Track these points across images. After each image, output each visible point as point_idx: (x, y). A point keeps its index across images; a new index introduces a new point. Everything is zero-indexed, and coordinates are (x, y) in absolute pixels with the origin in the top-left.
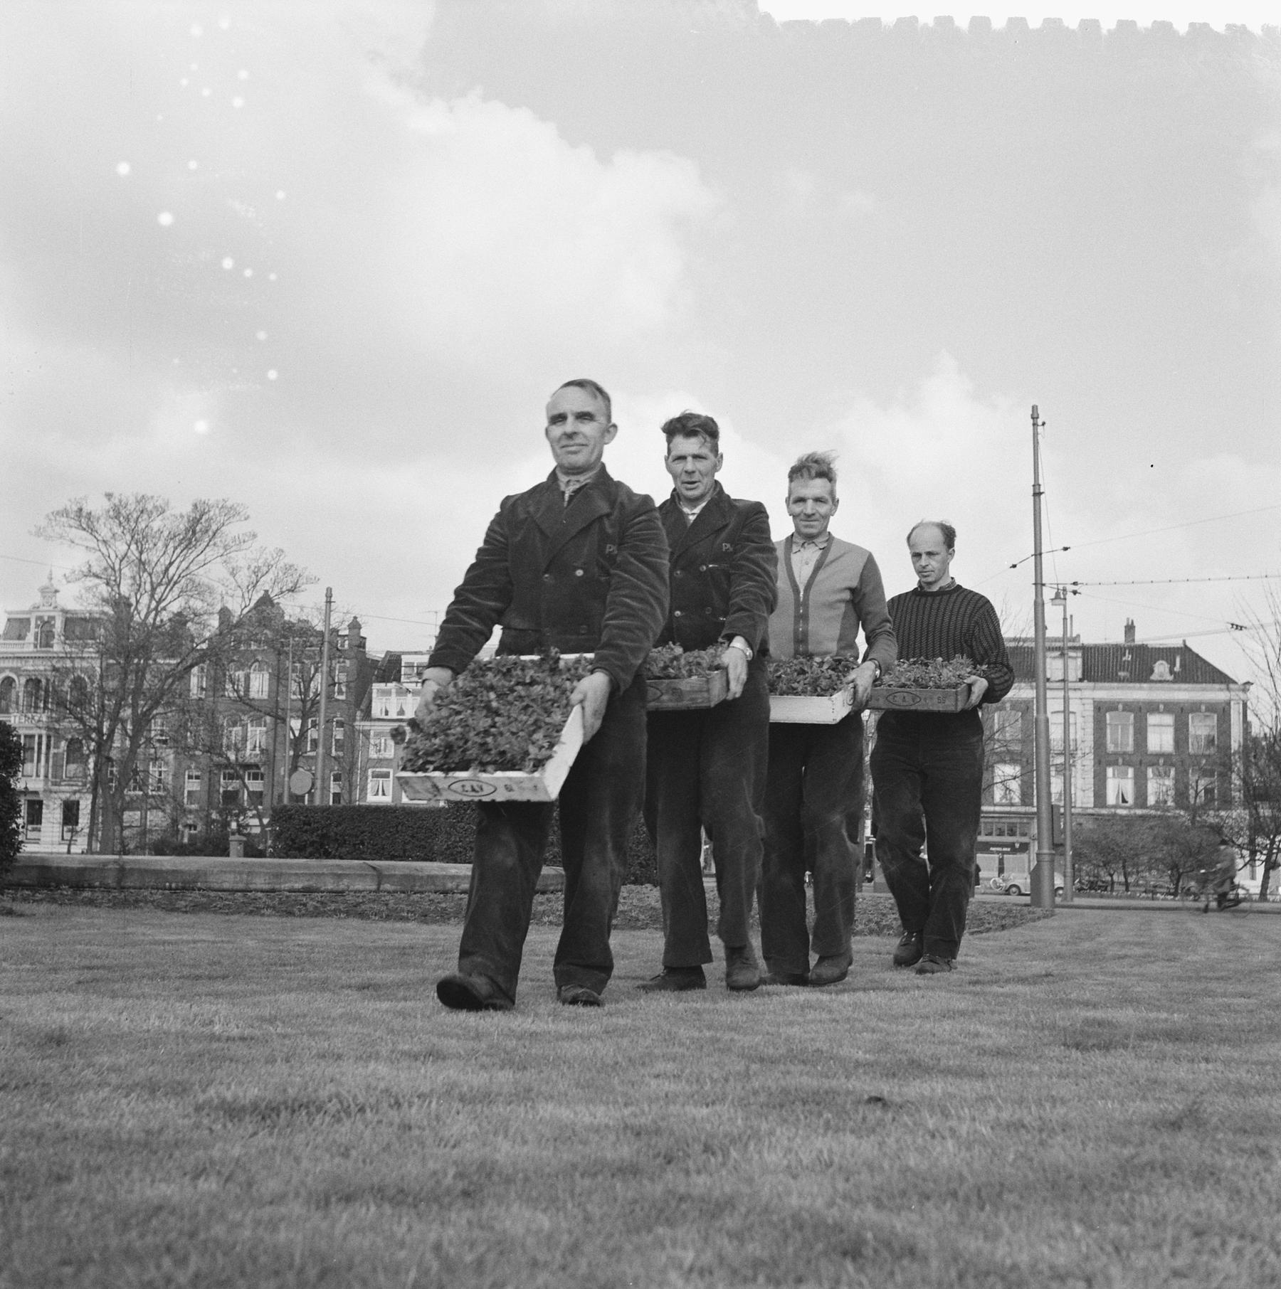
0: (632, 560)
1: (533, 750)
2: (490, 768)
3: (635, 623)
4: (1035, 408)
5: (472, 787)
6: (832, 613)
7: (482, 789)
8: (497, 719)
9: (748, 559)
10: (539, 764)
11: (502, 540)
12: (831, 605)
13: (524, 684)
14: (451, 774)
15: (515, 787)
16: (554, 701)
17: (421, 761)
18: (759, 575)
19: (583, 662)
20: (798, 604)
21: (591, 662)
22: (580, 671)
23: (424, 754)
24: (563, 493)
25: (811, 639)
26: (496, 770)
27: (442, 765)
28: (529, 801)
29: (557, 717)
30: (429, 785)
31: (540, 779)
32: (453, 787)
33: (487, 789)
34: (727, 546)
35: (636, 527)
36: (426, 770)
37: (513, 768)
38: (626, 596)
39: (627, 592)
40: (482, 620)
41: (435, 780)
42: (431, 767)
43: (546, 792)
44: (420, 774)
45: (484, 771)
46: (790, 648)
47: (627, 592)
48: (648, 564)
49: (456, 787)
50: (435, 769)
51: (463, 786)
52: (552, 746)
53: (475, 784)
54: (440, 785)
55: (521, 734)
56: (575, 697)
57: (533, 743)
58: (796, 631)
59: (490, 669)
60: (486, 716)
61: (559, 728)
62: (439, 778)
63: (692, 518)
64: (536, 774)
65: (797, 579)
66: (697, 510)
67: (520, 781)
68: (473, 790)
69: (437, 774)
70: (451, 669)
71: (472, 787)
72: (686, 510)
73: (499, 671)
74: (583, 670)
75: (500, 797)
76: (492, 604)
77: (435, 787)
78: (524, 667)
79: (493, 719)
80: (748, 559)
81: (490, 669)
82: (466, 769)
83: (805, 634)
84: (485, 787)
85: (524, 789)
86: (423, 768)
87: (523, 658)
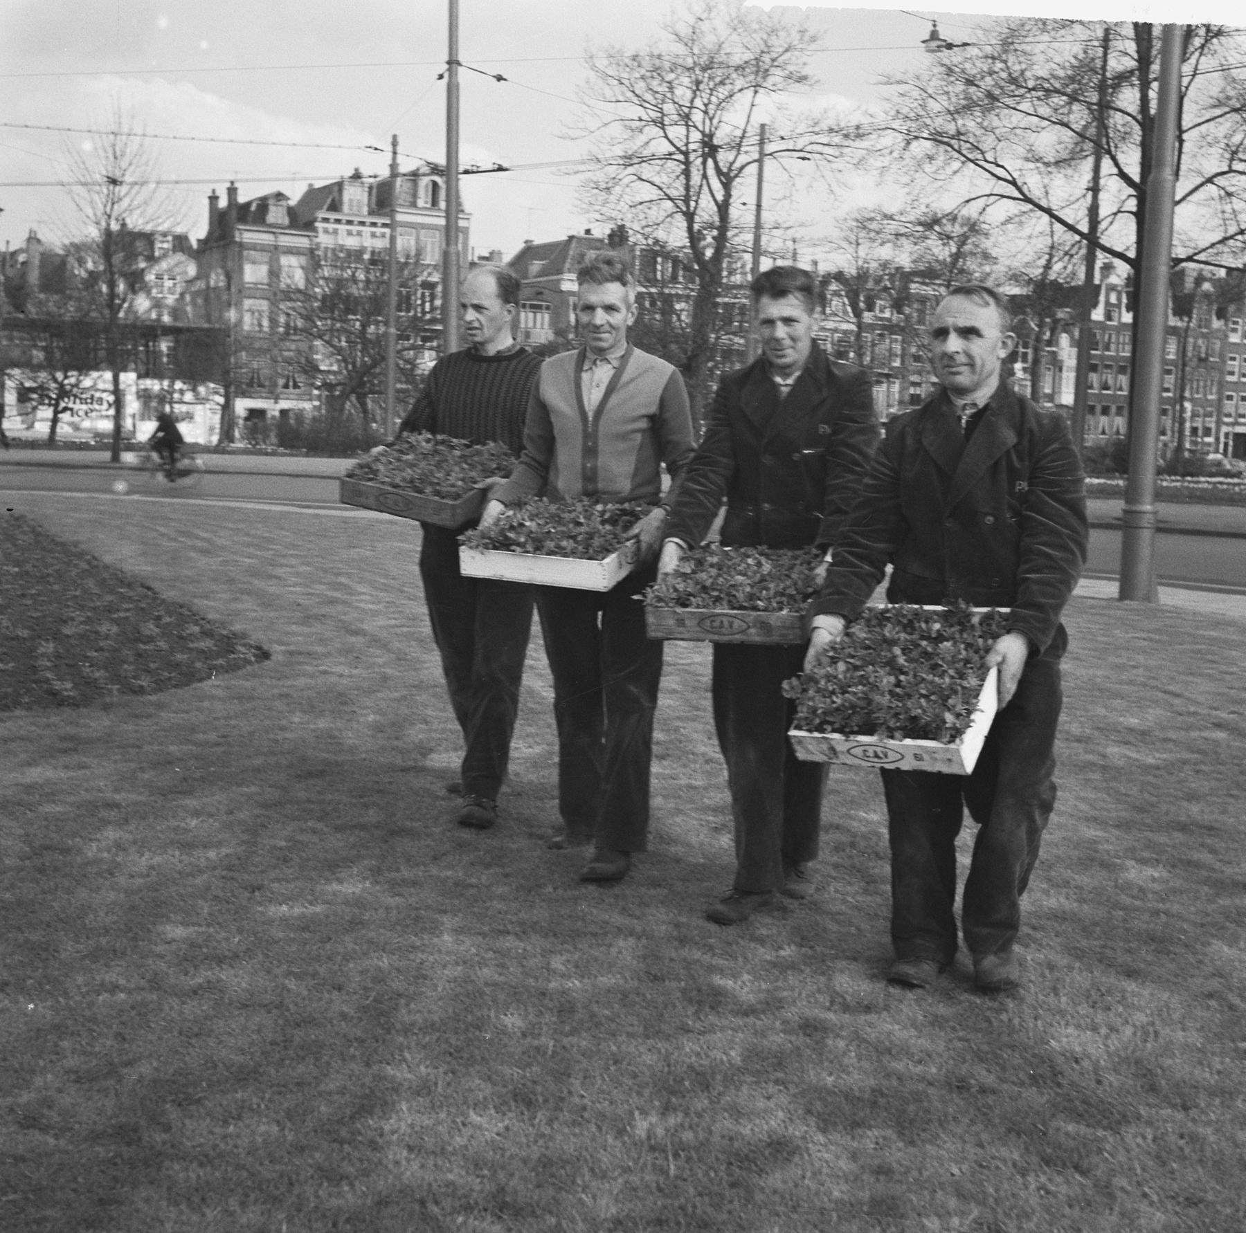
0: (1047, 499)
1: (949, 717)
2: (897, 734)
3: (1058, 576)
4: (395, 137)
5: (875, 752)
6: (622, 446)
7: (886, 756)
8: (902, 678)
9: (848, 446)
10: (956, 734)
11: (888, 472)
12: (623, 437)
13: (928, 638)
14: (852, 737)
15: (926, 757)
16: (967, 661)
17: (817, 721)
18: (859, 465)
19: (997, 617)
20: (586, 436)
21: (1005, 617)
22: (994, 627)
23: (824, 713)
24: (960, 418)
25: (601, 474)
26: (905, 737)
27: (844, 727)
28: (940, 772)
29: (972, 681)
30: (825, 747)
31: (958, 751)
32: (853, 751)
33: (892, 756)
34: (825, 429)
35: (1049, 458)
36: (822, 731)
37: (925, 737)
38: (1045, 544)
39: (1045, 538)
40: (871, 564)
41: (833, 743)
42: (829, 728)
43: (962, 765)
44: (816, 734)
45: (892, 737)
46: (578, 486)
47: (1045, 538)
48: (1063, 502)
49: (858, 751)
50: (834, 731)
51: (865, 751)
52: (969, 712)
53: (878, 750)
54: (839, 748)
55: (933, 697)
56: (993, 659)
57: (949, 710)
58: (584, 468)
59: (888, 619)
60: (889, 674)
61: (976, 693)
62: (838, 742)
63: (785, 390)
64: (952, 746)
65: (587, 408)
66: (790, 381)
67: (932, 752)
68: (876, 756)
69: (836, 736)
70: (844, 617)
71: (875, 752)
72: (778, 380)
73: (899, 622)
74: (998, 626)
75: (906, 765)
76: (881, 546)
77: (832, 749)
78: (928, 618)
79: (897, 677)
80: (848, 446)
81: (888, 619)
82: (870, 732)
83: (594, 470)
84: (890, 753)
85: (936, 759)
86: (820, 729)
87: (926, 607)
